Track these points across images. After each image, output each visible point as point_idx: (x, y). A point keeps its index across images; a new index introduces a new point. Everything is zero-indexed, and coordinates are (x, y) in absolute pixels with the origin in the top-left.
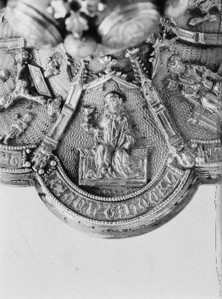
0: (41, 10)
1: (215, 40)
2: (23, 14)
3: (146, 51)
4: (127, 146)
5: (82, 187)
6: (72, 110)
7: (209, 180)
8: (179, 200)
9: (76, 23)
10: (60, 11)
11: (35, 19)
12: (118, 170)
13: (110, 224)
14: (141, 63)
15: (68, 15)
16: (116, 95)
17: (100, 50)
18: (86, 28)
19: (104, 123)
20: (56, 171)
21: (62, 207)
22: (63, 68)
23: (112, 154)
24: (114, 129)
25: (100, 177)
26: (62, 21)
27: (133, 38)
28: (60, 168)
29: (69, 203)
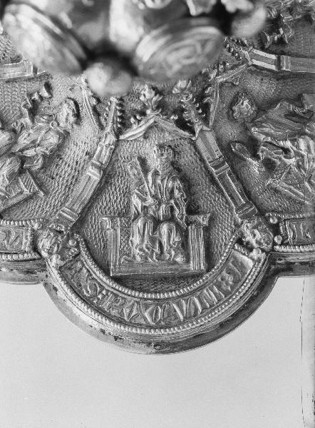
1: (307, 66)
2: (32, 21)
11: (47, 30)
13: (147, 332)
20: (81, 257)
21: (90, 312)
22: (86, 112)
27: (184, 66)
28: (85, 255)
29: (114, 312)
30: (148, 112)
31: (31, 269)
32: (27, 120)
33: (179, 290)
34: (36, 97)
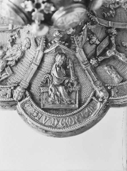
3: (78, 29)
4: (9, 63)
9: (37, 15)
10: (29, 7)
15: (33, 11)
17: (53, 29)
18: (43, 19)
26: (30, 13)
30: (46, 29)
31: (12, 105)
32: (10, 46)
33: (56, 115)
34: (14, 37)
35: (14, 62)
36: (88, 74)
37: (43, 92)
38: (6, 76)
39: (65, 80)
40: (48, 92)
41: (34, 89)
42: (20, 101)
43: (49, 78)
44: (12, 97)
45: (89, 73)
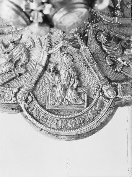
0: (18, 4)
1: (128, 21)
4: (75, 86)
5: (48, 110)
6: (43, 66)
7: (126, 104)
8: (103, 120)
11: (14, 10)
12: (70, 99)
14: (80, 36)
16: (69, 55)
19: (62, 72)
20: (31, 105)
23: (66, 90)
24: (67, 76)
25: (59, 104)
35: (77, 80)
36: (94, 72)
37: (122, 70)
38: (86, 95)
39: (121, 46)
40: (124, 65)
41: (112, 75)
42: (117, 94)
43: (111, 57)
44: (109, 99)
45: (95, 71)
